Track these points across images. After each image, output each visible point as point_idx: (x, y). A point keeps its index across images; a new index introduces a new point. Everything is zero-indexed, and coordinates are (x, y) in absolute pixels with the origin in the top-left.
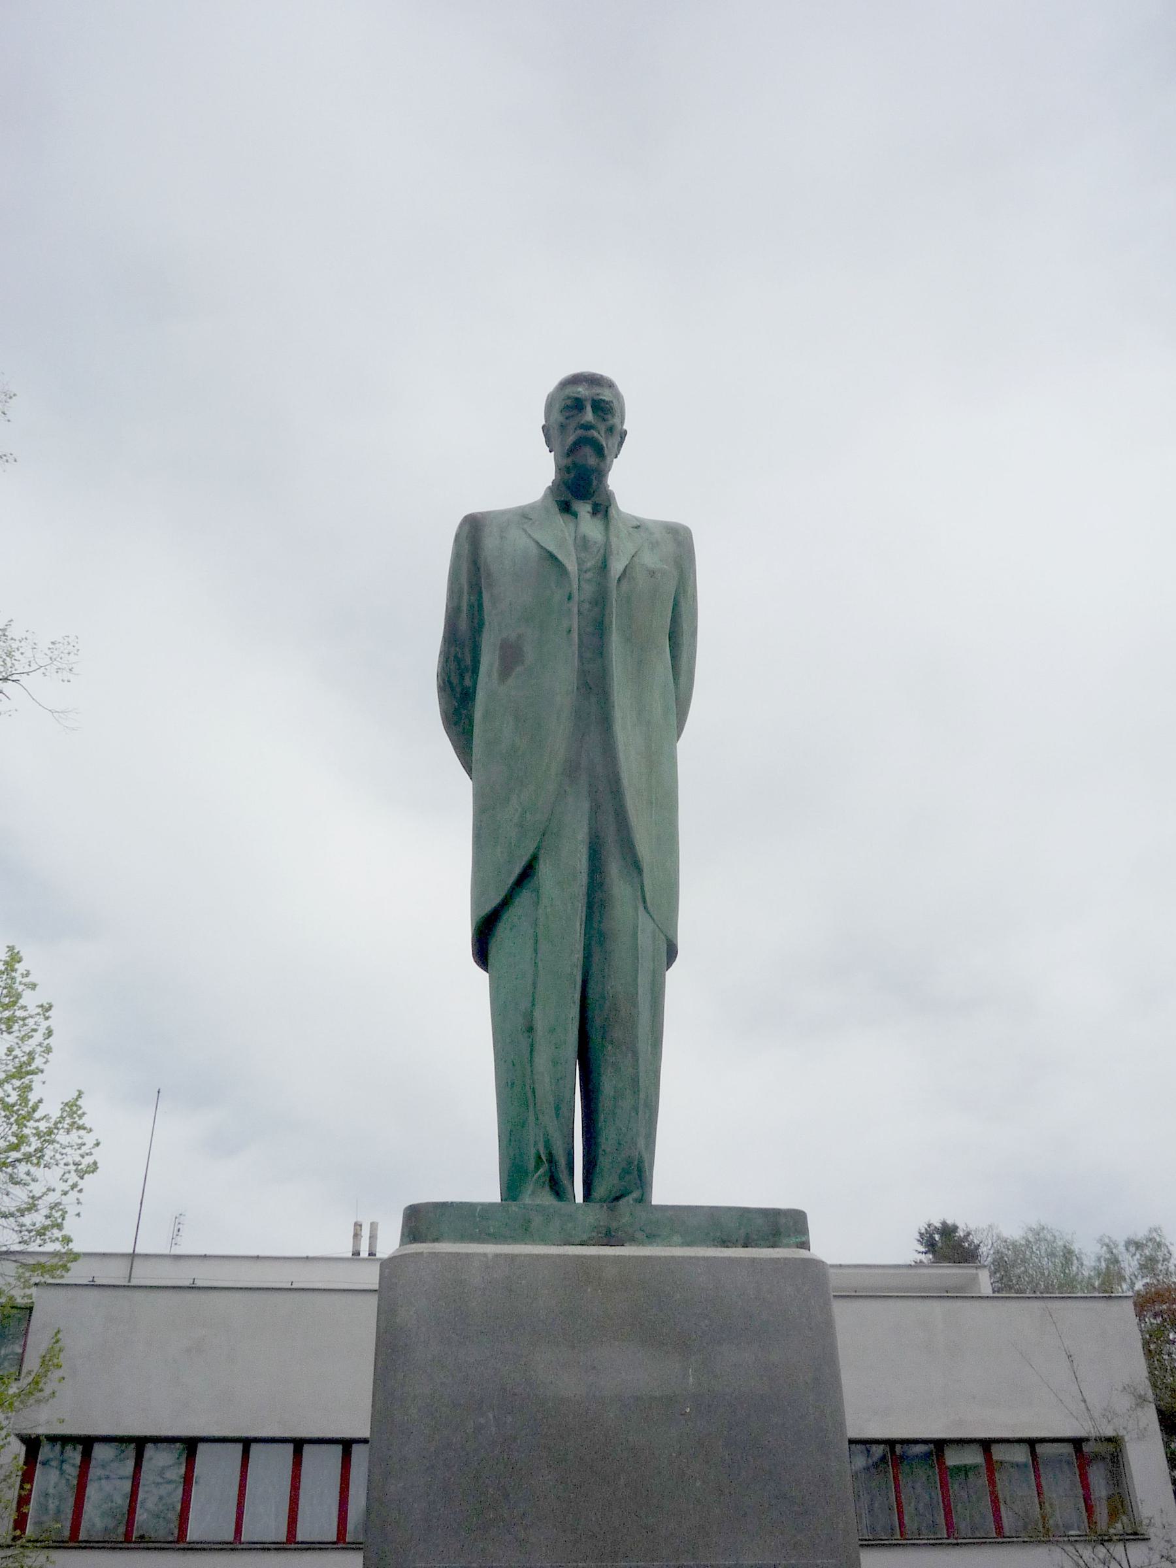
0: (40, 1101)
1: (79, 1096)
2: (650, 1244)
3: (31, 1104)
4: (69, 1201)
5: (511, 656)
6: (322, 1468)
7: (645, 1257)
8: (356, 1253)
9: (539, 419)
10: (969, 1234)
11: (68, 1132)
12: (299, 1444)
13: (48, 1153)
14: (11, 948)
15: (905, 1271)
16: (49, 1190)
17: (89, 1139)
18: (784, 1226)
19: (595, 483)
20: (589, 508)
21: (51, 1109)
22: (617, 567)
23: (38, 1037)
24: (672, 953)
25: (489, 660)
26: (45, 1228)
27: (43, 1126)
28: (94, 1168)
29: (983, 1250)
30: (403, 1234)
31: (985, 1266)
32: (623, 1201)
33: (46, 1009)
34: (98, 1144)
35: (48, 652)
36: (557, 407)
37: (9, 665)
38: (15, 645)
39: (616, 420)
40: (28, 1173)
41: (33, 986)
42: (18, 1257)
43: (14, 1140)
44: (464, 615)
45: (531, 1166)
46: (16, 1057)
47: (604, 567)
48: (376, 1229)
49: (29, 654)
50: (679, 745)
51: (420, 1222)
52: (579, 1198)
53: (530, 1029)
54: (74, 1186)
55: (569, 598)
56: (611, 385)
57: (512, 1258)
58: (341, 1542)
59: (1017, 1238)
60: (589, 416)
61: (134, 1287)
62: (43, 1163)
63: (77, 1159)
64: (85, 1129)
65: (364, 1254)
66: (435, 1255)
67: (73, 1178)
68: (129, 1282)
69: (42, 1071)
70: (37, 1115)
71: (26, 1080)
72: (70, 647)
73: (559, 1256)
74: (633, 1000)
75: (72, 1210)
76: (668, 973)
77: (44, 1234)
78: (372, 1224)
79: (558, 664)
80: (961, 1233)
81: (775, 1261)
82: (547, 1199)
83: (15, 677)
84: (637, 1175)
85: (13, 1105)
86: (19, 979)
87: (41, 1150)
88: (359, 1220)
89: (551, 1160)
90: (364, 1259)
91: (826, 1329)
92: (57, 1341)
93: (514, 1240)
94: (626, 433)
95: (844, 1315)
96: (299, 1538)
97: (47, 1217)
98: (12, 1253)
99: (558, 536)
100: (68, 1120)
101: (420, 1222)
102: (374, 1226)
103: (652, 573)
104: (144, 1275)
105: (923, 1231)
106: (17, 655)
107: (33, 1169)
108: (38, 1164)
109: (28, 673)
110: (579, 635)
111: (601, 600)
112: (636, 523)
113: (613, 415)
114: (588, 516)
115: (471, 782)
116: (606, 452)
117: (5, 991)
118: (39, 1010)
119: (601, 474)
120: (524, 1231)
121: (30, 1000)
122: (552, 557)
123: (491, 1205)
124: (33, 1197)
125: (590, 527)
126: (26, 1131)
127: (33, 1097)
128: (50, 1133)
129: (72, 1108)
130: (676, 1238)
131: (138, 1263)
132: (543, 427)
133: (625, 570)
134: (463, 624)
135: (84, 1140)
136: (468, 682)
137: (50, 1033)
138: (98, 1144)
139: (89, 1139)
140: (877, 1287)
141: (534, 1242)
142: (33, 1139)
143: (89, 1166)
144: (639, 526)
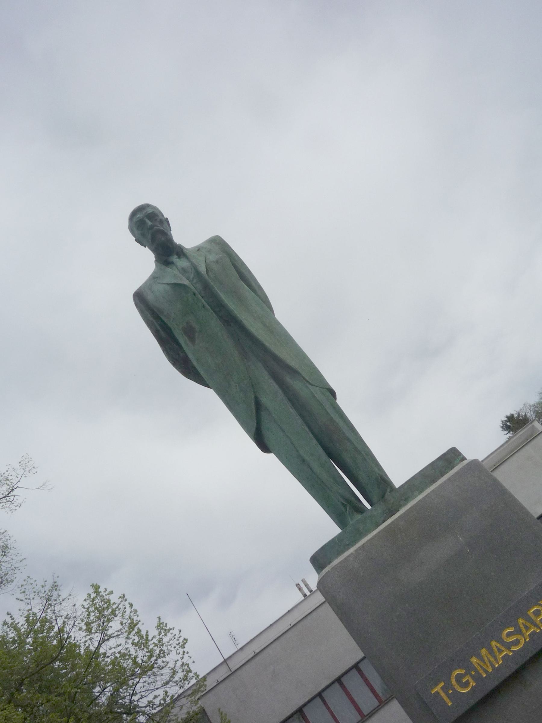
0: (147, 632)
1: (160, 619)
2: (408, 503)
3: (144, 636)
4: (186, 660)
5: (190, 332)
6: (354, 683)
7: (410, 509)
8: (305, 595)
9: (126, 223)
10: (519, 414)
11: (166, 635)
12: (339, 680)
13: (165, 648)
14: (92, 585)
15: (506, 445)
16: (176, 662)
17: (176, 632)
18: (452, 457)
19: (171, 246)
20: (175, 257)
21: (153, 632)
22: (202, 269)
23: (128, 610)
24: (333, 393)
25: (182, 339)
26: (185, 676)
27: (155, 641)
28: (186, 640)
29: (528, 415)
30: (316, 570)
31: (533, 421)
32: (386, 496)
33: (123, 597)
34: (180, 631)
35: (20, 467)
36: (135, 229)
37: (10, 484)
38: (6, 475)
39: (160, 217)
40: (163, 662)
41: (112, 593)
42: (185, 694)
43: (148, 654)
44: (161, 331)
45: (341, 508)
46: (125, 623)
47: (198, 273)
48: (305, 581)
49: (14, 473)
50: (276, 316)
51: (319, 561)
52: (369, 507)
53: (303, 461)
54: (184, 652)
55: (194, 294)
56: (148, 206)
57: (363, 547)
58: (382, 703)
59: (538, 401)
60: (149, 223)
61: (234, 672)
62: (166, 654)
63: (178, 642)
64: (171, 629)
65: (308, 593)
66: (334, 568)
67: (181, 651)
68: (231, 671)
69: (140, 621)
70: (150, 638)
71: (136, 630)
72: (27, 459)
73: (379, 533)
74: (332, 421)
75: (190, 662)
76: (338, 401)
77: (187, 678)
78: (302, 580)
79: (209, 321)
80: (516, 416)
81: (458, 473)
82: (359, 517)
83: (15, 487)
84: (383, 481)
85: (139, 642)
86: (104, 594)
87: (161, 650)
88: (297, 582)
89: (349, 502)
90: (309, 596)
91: (496, 483)
92: (222, 713)
93: (358, 540)
94: (167, 219)
95: (498, 475)
96: (365, 714)
97: (183, 671)
98: (181, 694)
99: (172, 276)
100: (163, 631)
101: (319, 561)
102: (304, 581)
103: (217, 262)
104: (234, 665)
105: (502, 425)
106: (10, 478)
107: (164, 659)
108: (164, 656)
109: (19, 481)
110: (209, 305)
111: (206, 287)
112: (197, 249)
113: (158, 216)
114: (178, 260)
115: (212, 390)
116: (166, 231)
117: (103, 603)
118: (121, 599)
119: (170, 240)
120: (359, 534)
121: (114, 599)
122: (176, 285)
123: (340, 534)
124: (172, 669)
125: (182, 263)
126: (151, 647)
127: (143, 633)
128: (159, 641)
129: (161, 626)
130: (416, 493)
131: (229, 663)
132: (136, 240)
133: (206, 269)
134: (163, 335)
135: (174, 634)
136: (182, 354)
137: (131, 605)
138: (180, 631)
139: (176, 632)
140: (502, 457)
141: (366, 535)
142: (155, 648)
143: (183, 642)
144: (199, 249)
